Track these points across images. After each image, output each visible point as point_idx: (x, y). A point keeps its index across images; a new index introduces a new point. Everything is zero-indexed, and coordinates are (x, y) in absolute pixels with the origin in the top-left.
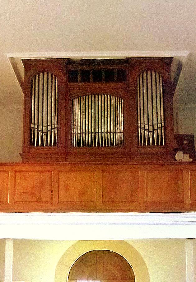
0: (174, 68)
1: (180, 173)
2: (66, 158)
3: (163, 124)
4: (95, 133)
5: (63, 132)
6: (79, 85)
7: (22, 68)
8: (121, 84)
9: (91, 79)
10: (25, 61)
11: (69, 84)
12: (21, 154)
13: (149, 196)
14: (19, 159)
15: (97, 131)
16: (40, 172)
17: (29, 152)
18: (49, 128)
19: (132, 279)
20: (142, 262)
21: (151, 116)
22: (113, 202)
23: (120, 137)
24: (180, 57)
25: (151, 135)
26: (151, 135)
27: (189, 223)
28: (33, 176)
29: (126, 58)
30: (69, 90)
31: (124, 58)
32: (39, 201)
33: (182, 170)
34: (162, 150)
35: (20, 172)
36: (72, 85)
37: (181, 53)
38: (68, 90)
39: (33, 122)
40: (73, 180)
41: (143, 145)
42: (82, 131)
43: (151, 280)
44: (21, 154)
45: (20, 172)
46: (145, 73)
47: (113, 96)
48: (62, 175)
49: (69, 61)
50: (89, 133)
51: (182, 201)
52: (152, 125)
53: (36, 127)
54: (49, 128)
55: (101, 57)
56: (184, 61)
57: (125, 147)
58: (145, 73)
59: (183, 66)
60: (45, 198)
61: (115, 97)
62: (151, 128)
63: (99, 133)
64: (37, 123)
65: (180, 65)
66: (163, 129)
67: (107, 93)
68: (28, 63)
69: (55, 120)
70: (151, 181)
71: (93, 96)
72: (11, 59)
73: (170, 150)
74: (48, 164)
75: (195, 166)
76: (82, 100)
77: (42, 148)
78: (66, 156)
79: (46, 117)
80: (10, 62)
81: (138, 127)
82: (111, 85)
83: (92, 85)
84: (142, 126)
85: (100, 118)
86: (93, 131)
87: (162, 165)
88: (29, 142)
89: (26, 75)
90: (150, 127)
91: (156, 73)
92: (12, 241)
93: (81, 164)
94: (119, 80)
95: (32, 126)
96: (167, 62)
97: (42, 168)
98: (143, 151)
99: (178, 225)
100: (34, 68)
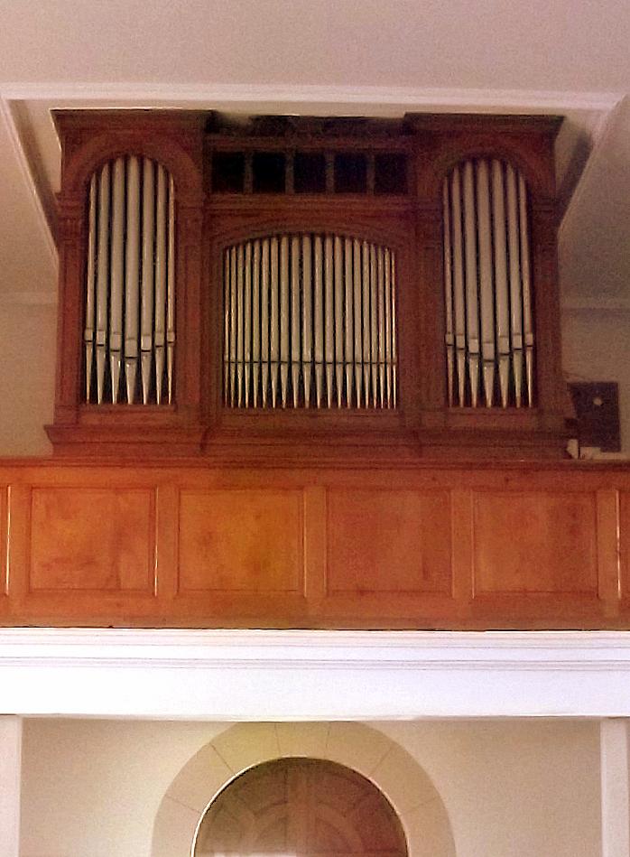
0: (563, 148)
1: (586, 501)
2: (203, 446)
3: (530, 338)
4: (313, 362)
5: (193, 356)
6: (247, 201)
7: (52, 145)
8: (393, 204)
9: (331, 181)
10: (61, 117)
11: (218, 196)
12: (47, 428)
13: (483, 572)
14: (43, 447)
15: (307, 355)
16: (118, 490)
17: (77, 423)
18: (146, 343)
19: (393, 850)
20: (430, 799)
21: (488, 311)
22: (362, 592)
23: (386, 379)
24: (588, 112)
25: (130, 370)
26: (130, 370)
27: (608, 666)
28: (90, 502)
29: (406, 115)
30: (213, 216)
31: (401, 114)
32: (112, 587)
33: (594, 493)
34: (530, 422)
35: (49, 488)
36: (226, 201)
37: (590, 102)
38: (210, 219)
39: (450, 328)
40: (234, 520)
41: (505, 403)
42: (233, 356)
43: (410, 855)
44: (47, 428)
45: (49, 488)
46: (469, 170)
47: (361, 242)
48: (192, 504)
49: (212, 122)
50: (280, 362)
51: (594, 594)
52: (507, 334)
53: (101, 338)
54: (146, 343)
55: (156, 101)
56: (598, 130)
57: (402, 415)
58: (469, 170)
59: (595, 148)
60: (131, 577)
61: (353, 242)
62: (489, 352)
63: (313, 362)
64: (92, 326)
65: (583, 148)
66: (170, 349)
67: (341, 232)
68: (74, 125)
69: (165, 317)
70: (494, 524)
71: (295, 243)
72: (18, 107)
73: (553, 422)
74: (145, 462)
75: (626, 476)
76: (241, 256)
77: (119, 412)
78: (205, 437)
79: (121, 304)
80: (10, 117)
81: (446, 345)
82: (355, 202)
83: (295, 203)
84: (461, 343)
85: (321, 312)
86: (295, 356)
87: (525, 470)
88: (79, 389)
89: (66, 163)
90: (484, 345)
91: (504, 171)
92: (20, 721)
93: (256, 465)
94: (383, 188)
95: (89, 335)
96: (539, 132)
97: (128, 475)
98: (461, 423)
99: (559, 674)
100: (95, 144)
